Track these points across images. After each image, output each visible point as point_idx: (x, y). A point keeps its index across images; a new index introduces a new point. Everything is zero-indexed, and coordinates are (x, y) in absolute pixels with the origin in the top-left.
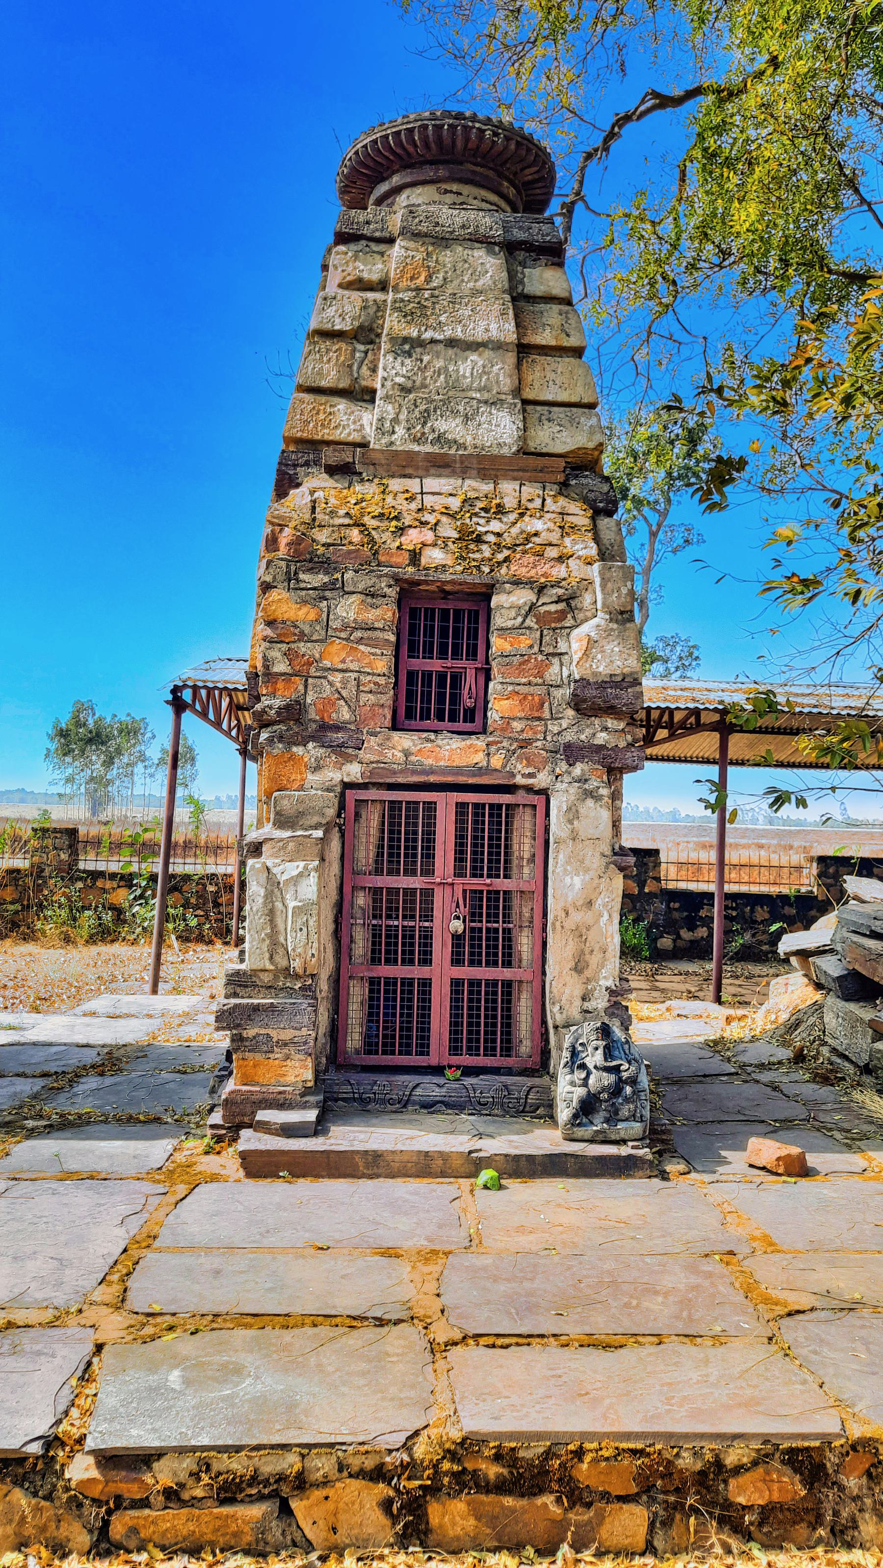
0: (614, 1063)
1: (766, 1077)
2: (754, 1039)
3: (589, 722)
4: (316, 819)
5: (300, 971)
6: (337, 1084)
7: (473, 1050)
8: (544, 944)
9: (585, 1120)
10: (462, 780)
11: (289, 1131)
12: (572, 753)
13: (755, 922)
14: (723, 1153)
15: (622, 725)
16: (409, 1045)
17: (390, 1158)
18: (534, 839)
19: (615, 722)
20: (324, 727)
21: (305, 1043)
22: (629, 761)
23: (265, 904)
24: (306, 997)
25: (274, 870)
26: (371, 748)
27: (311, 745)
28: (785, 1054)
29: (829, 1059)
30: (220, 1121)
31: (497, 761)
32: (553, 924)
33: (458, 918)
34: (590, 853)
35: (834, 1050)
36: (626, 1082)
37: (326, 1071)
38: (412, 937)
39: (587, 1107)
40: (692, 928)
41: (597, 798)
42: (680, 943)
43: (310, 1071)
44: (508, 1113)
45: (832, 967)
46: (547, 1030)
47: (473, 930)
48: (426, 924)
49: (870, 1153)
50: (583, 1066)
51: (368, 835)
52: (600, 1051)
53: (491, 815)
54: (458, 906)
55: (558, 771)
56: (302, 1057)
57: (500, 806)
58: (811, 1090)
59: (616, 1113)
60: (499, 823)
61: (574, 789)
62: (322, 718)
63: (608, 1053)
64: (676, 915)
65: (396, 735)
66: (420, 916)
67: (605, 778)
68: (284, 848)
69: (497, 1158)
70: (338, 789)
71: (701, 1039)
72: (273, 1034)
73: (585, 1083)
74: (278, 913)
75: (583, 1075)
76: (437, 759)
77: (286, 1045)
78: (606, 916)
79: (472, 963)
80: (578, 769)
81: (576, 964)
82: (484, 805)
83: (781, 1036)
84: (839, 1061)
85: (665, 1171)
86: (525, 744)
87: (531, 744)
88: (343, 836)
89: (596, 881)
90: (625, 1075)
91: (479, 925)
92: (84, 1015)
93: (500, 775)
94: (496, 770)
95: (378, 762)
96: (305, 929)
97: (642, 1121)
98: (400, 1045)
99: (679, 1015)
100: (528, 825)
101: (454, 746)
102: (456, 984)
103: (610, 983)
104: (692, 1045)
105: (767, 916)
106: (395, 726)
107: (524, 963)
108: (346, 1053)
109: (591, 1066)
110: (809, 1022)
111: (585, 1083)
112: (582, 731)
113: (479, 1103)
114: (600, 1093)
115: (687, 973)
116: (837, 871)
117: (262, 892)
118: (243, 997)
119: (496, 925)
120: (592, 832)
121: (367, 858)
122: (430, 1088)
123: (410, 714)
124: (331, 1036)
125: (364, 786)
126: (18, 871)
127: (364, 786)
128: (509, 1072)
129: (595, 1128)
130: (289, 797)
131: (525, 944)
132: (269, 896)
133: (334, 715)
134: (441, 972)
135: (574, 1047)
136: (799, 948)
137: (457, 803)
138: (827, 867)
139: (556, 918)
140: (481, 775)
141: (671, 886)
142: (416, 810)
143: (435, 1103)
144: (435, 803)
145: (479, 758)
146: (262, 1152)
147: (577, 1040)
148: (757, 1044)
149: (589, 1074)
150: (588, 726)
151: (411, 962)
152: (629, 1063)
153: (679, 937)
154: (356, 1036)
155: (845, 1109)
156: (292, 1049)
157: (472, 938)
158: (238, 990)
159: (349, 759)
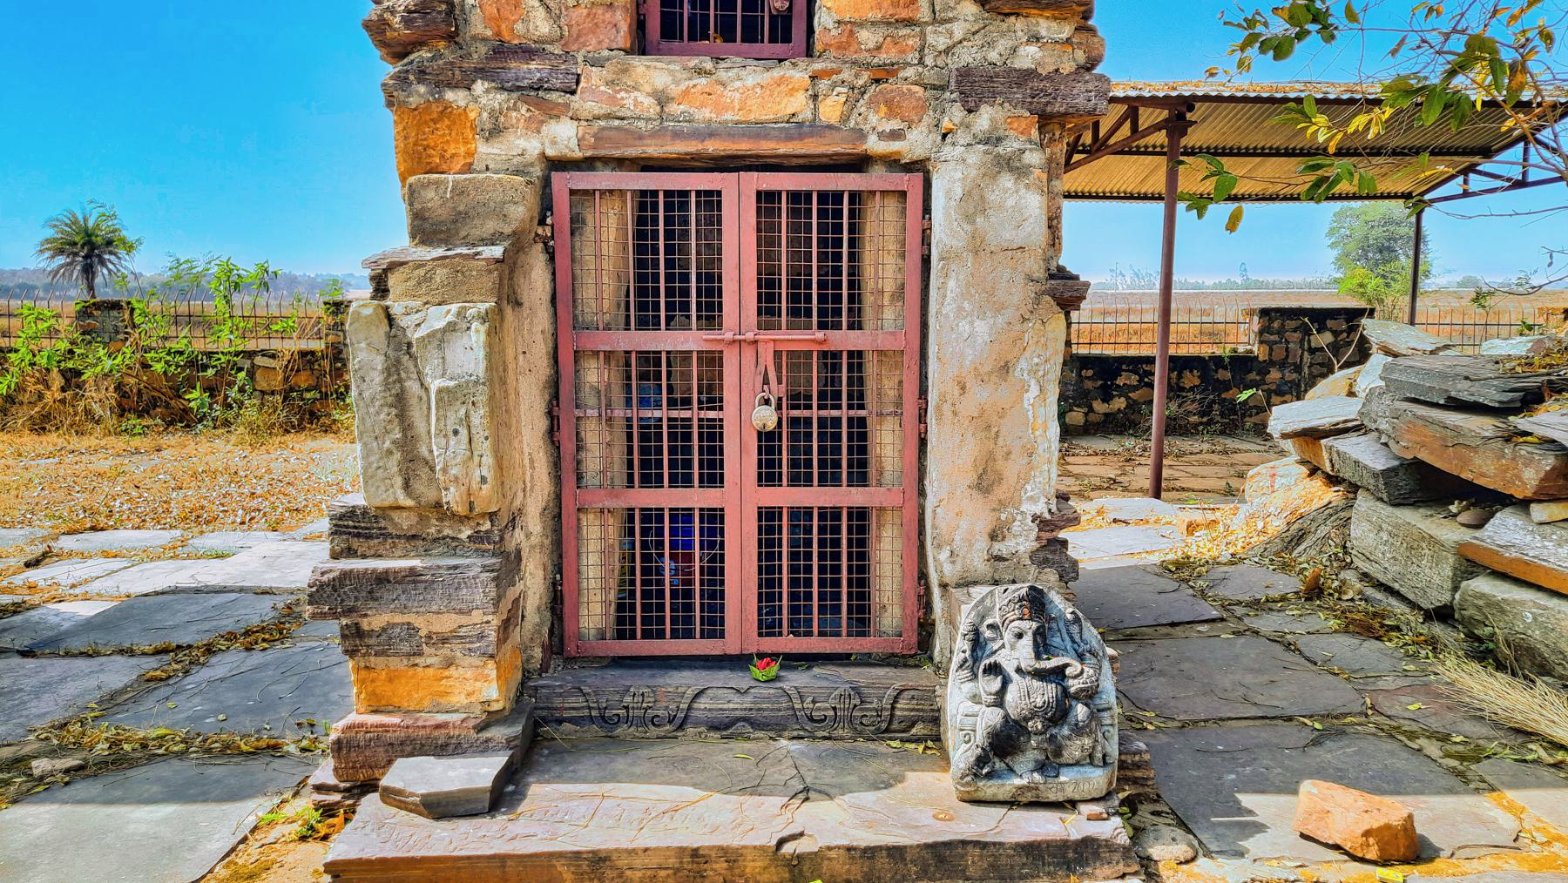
0: (1054, 662)
1: (1267, 623)
2: (1235, 560)
3: (1004, 26)
4: (491, 226)
5: (461, 510)
6: (560, 695)
7: (799, 627)
8: (923, 442)
9: (999, 765)
10: (766, 147)
11: (440, 808)
12: (973, 87)
13: (1183, 389)
14: (1246, 800)
15: (1066, 31)
16: (689, 620)
17: (623, 862)
18: (903, 256)
19: (1054, 25)
20: (503, 51)
21: (481, 637)
22: (1080, 101)
23: (387, 385)
24: (482, 553)
25: (404, 322)
26: (593, 91)
27: (479, 87)
28: (1288, 584)
29: (1360, 592)
30: (332, 780)
31: (830, 110)
32: (938, 408)
33: (767, 402)
34: (1007, 276)
35: (1365, 576)
36: (1076, 697)
37: (544, 668)
38: (687, 437)
39: (1004, 744)
40: (1107, 399)
41: (1020, 171)
42: (1092, 417)
43: (494, 685)
44: (860, 734)
45: (1365, 454)
46: (928, 588)
47: (794, 422)
48: (712, 414)
49: (1510, 795)
50: (995, 669)
51: (598, 256)
52: (1028, 641)
53: (822, 214)
54: (766, 382)
55: (946, 124)
56: (477, 661)
57: (838, 196)
58: (1346, 648)
59: (1058, 752)
60: (838, 228)
61: (976, 156)
62: (498, 34)
63: (1042, 646)
64: (1089, 385)
65: (639, 63)
66: (700, 402)
67: (1035, 133)
68: (427, 279)
69: (833, 854)
70: (537, 171)
71: (1155, 559)
72: (418, 621)
73: (999, 699)
74: (414, 401)
75: (996, 684)
76: (720, 108)
77: (445, 641)
78: (1034, 390)
79: (795, 481)
80: (985, 118)
81: (980, 477)
82: (809, 195)
83: (1277, 554)
84: (1379, 596)
85: (1149, 858)
86: (883, 74)
87: (894, 73)
88: (552, 258)
89: (1018, 327)
90: (1074, 685)
91: (806, 413)
92: (305, 539)
93: (837, 136)
94: (830, 127)
95: (608, 116)
96: (463, 432)
97: (1105, 764)
98: (674, 620)
99: (1115, 521)
100: (891, 231)
101: (750, 82)
102: (768, 517)
103: (1040, 508)
104: (1144, 569)
105: (1197, 382)
106: (640, 45)
107: (888, 477)
108: (580, 637)
109: (1009, 668)
110: (1320, 534)
111: (999, 699)
112: (990, 44)
113: (811, 719)
114: (1026, 719)
115: (1104, 453)
116: (1283, 325)
117: (379, 362)
118: (364, 557)
119: (835, 413)
120: (1009, 236)
121: (599, 298)
122: (723, 693)
123: (670, 31)
124: (553, 610)
125: (587, 164)
126: (313, 353)
127: (587, 164)
128: (866, 661)
129: (1017, 782)
130: (437, 183)
131: (887, 444)
132: (393, 370)
133: (519, 27)
134: (740, 497)
135: (976, 632)
136: (1306, 425)
137: (759, 193)
138: (1271, 321)
139: (943, 399)
140: (801, 137)
141: (1083, 351)
142: (684, 206)
143: (735, 721)
144: (719, 193)
145: (798, 104)
146: (369, 862)
147: (983, 618)
148: (1240, 567)
149: (1006, 682)
150: (1003, 34)
151: (687, 481)
152: (1081, 657)
153: (1091, 409)
154: (597, 608)
155: (1427, 691)
156: (457, 649)
157: (794, 437)
158: (355, 543)
159: (553, 113)
